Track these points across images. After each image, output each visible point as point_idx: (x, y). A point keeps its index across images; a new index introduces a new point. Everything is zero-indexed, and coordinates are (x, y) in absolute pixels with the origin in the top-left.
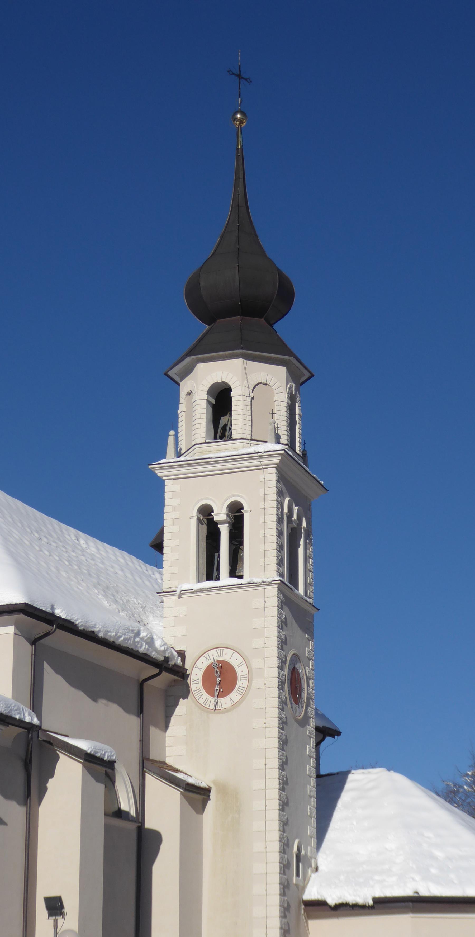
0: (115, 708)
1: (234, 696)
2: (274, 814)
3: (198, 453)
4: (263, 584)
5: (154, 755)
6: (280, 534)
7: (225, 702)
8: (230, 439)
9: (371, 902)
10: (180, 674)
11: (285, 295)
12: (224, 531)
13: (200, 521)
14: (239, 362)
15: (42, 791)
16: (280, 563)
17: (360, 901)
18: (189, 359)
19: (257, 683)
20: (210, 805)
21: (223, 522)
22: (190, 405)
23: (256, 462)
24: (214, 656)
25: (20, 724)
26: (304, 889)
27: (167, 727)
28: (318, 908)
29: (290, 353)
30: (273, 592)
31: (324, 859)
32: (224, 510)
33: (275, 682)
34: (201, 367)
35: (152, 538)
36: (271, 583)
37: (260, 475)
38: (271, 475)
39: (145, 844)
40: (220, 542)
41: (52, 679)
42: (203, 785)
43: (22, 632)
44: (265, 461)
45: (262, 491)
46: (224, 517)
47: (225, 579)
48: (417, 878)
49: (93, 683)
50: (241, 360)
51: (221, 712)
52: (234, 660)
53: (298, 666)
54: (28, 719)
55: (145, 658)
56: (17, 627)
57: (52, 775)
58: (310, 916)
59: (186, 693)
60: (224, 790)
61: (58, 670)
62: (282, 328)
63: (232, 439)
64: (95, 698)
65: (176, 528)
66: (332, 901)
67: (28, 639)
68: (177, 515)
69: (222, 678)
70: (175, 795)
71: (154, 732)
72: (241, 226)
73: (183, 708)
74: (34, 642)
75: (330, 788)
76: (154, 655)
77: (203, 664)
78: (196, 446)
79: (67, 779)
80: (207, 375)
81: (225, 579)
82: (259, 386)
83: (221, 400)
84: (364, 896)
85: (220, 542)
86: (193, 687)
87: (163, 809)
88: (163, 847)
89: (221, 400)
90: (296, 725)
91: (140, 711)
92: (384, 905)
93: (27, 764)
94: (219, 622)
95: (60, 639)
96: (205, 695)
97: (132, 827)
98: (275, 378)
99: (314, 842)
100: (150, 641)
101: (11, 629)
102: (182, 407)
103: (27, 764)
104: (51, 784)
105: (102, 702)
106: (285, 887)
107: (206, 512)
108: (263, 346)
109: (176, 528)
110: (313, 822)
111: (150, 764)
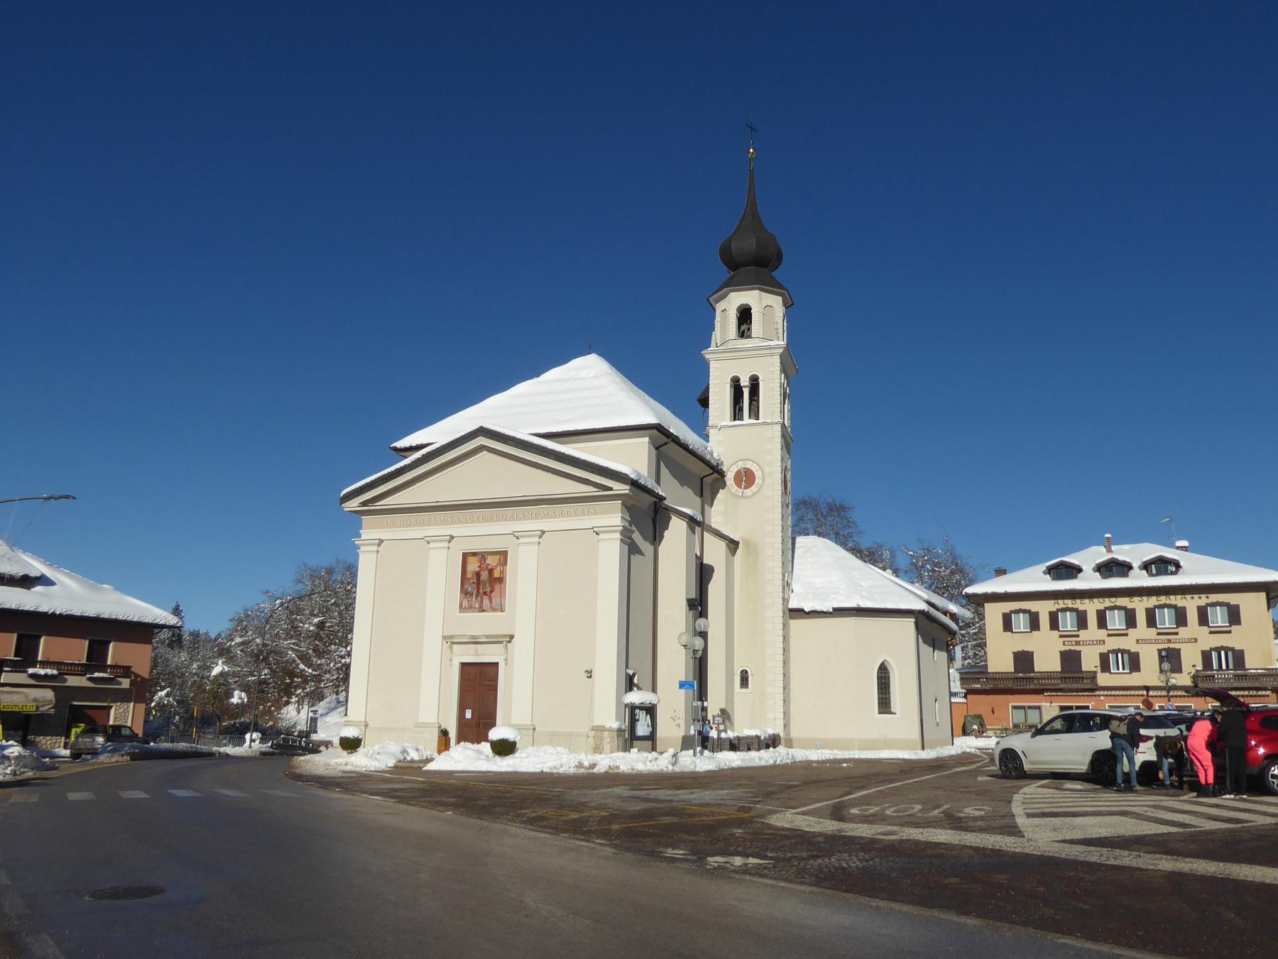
1: (754, 488)
3: (731, 345)
4: (772, 423)
7: (748, 492)
8: (750, 337)
10: (722, 474)
11: (779, 258)
14: (757, 292)
17: (825, 610)
19: (768, 481)
22: (725, 318)
24: (741, 465)
28: (797, 613)
29: (781, 287)
37: (770, 359)
38: (777, 360)
43: (652, 442)
47: (747, 420)
49: (682, 476)
52: (754, 468)
55: (707, 463)
59: (724, 485)
60: (747, 543)
63: (750, 340)
66: (807, 610)
69: (746, 478)
73: (721, 494)
74: (657, 448)
77: (734, 469)
78: (481, 441)
80: (736, 299)
81: (747, 420)
82: (767, 307)
83: (745, 315)
84: (827, 606)
85: (745, 397)
87: (715, 553)
89: (745, 315)
91: (701, 496)
92: (839, 612)
94: (748, 445)
95: (672, 448)
98: (776, 302)
100: (712, 454)
101: (647, 439)
102: (718, 319)
103: (654, 521)
104: (666, 533)
107: (736, 383)
108: (769, 284)
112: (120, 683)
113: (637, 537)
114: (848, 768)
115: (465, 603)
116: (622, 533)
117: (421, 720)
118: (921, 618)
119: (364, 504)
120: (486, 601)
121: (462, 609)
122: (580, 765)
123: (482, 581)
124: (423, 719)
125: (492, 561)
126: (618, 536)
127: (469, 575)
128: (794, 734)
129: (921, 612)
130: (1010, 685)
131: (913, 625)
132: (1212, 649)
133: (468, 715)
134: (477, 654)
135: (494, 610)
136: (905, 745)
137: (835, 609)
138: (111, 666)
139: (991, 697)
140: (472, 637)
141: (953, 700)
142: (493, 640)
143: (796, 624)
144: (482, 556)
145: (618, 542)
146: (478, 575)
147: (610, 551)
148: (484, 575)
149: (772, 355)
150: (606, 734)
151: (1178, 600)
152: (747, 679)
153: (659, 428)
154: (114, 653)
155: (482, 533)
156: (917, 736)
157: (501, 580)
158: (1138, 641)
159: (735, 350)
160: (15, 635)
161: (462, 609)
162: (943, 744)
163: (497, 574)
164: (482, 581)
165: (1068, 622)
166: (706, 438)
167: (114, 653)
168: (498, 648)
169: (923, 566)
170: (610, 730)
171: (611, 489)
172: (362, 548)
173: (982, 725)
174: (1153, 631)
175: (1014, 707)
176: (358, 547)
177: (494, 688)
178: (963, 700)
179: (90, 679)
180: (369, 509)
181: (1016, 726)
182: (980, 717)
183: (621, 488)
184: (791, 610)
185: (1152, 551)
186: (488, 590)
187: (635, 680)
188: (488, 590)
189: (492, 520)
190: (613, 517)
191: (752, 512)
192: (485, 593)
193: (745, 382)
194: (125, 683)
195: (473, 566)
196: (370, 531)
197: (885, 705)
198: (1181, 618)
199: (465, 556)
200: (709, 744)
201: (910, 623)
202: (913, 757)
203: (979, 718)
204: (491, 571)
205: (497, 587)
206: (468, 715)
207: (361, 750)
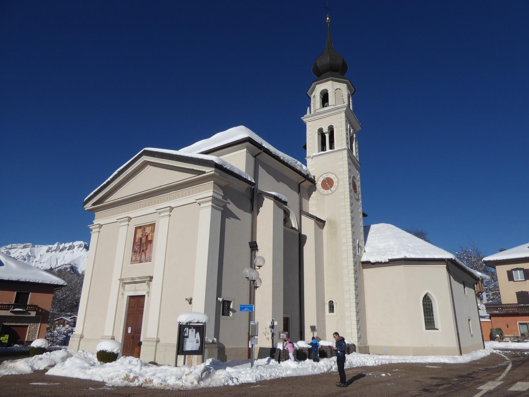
2: (349, 229)
5: (304, 209)
6: (347, 139)
9: (388, 261)
10: (313, 181)
12: (327, 136)
13: (319, 134)
15: (258, 212)
16: (347, 143)
19: (341, 183)
20: (325, 227)
21: (327, 133)
23: (338, 111)
24: (325, 176)
25: (246, 180)
26: (361, 258)
28: (367, 264)
30: (346, 152)
31: (367, 248)
33: (348, 182)
34: (317, 86)
36: (344, 149)
37: (339, 115)
38: (343, 115)
39: (302, 240)
40: (326, 140)
41: (262, 171)
43: (249, 151)
44: (341, 110)
45: (340, 120)
46: (327, 131)
48: (405, 252)
50: (331, 82)
52: (332, 177)
53: (355, 180)
54: (249, 179)
56: (247, 149)
57: (262, 206)
58: (364, 268)
61: (263, 167)
63: (330, 107)
64: (278, 181)
66: (372, 261)
67: (253, 156)
70: (312, 222)
71: (303, 199)
73: (314, 194)
74: (255, 157)
75: (366, 230)
76: (303, 172)
77: (321, 179)
79: (268, 205)
80: (320, 88)
81: (328, 150)
82: (338, 90)
85: (326, 140)
87: (308, 228)
88: (307, 241)
90: (355, 200)
91: (299, 192)
92: (393, 262)
93: (252, 201)
94: (330, 165)
97: (297, 233)
99: (363, 242)
102: (312, 102)
103: (252, 201)
104: (261, 209)
105: (281, 183)
106: (355, 255)
107: (321, 131)
110: (363, 235)
111: (302, 212)
112: (30, 314)
113: (232, 207)
114: (387, 380)
115: (133, 259)
116: (213, 202)
118: (449, 263)
119: (94, 204)
120: (143, 256)
121: (132, 262)
123: (142, 245)
124: (105, 334)
126: (210, 204)
127: (137, 241)
128: (371, 342)
129: (450, 260)
130: (516, 311)
131: (445, 269)
133: (129, 331)
134: (135, 290)
136: (447, 352)
138: (29, 305)
139: (506, 318)
140: (133, 279)
141: (482, 320)
143: (367, 272)
145: (210, 209)
146: (141, 239)
147: (205, 217)
148: (144, 239)
149: (340, 113)
152: (333, 307)
153: (249, 140)
154: (32, 298)
155: (141, 213)
156: (455, 345)
157: (151, 242)
159: (319, 114)
160: (16, 292)
162: (476, 348)
163: (149, 238)
164: (142, 245)
166: (305, 163)
167: (32, 298)
168: (144, 285)
169: (463, 258)
171: (204, 172)
172: (93, 231)
173: (501, 335)
175: (520, 324)
176: (91, 230)
177: (273, 315)
178: (489, 320)
179: (11, 312)
181: (523, 335)
182: (500, 330)
183: (209, 171)
184: (364, 263)
187: (231, 307)
188: (145, 248)
189: (149, 205)
190: (207, 191)
191: (334, 204)
192: (143, 251)
193: (326, 130)
194: (33, 314)
196: (100, 219)
197: (430, 323)
200: (276, 354)
201: (442, 269)
202: (452, 362)
203: (499, 331)
204: (147, 237)
205: (149, 246)
206: (129, 331)
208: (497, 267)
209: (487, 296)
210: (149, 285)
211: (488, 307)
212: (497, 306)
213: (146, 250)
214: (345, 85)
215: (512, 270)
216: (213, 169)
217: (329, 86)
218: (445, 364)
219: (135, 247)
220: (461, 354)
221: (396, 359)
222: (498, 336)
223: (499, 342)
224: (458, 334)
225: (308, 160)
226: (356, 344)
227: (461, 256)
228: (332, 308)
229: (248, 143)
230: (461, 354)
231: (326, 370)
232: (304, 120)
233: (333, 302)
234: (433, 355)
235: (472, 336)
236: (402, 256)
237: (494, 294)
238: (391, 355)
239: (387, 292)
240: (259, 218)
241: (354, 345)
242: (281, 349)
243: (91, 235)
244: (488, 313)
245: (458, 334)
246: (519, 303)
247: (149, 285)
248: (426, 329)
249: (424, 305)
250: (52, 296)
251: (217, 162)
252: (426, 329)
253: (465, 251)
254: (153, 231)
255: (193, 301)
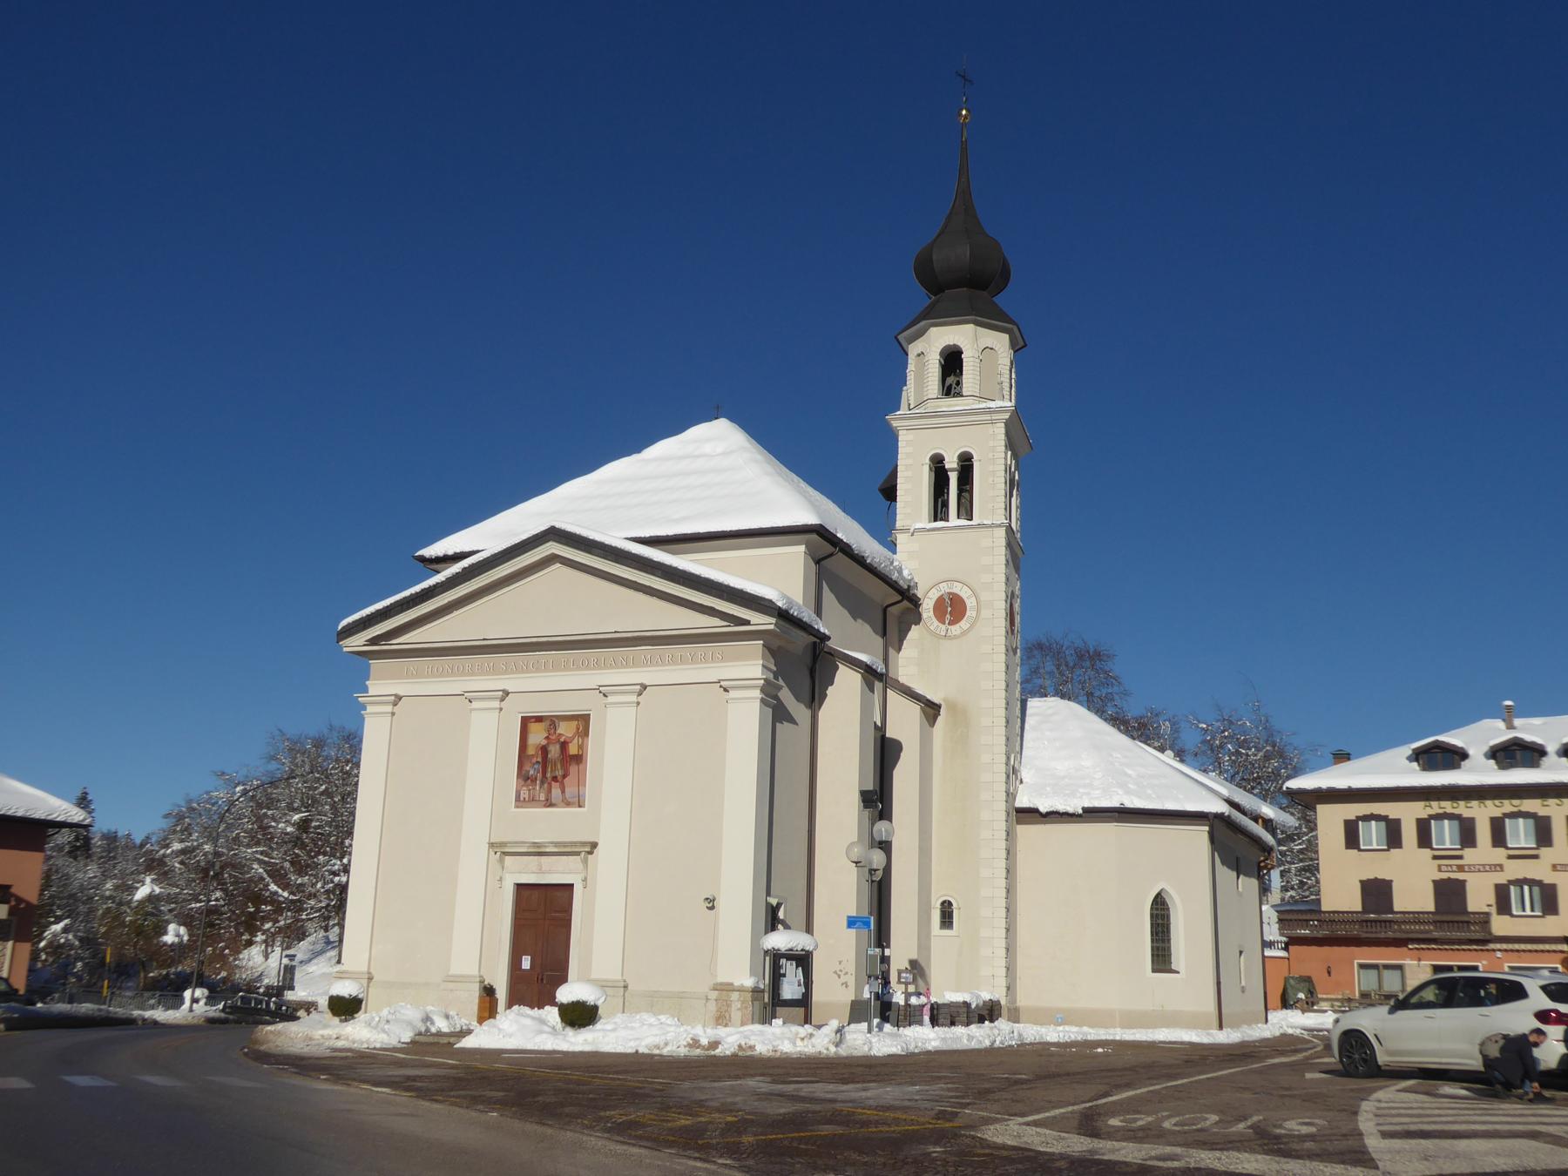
0: (867, 628)
1: (964, 624)
3: (931, 407)
4: (992, 526)
8: (959, 395)
10: (915, 602)
11: (1005, 275)
12: (953, 478)
14: (969, 328)
17: (1071, 810)
18: (923, 323)
19: (985, 613)
22: (922, 367)
23: (987, 417)
24: (944, 588)
27: (900, 649)
28: (1029, 815)
29: (1010, 321)
32: (955, 459)
34: (933, 330)
35: (880, 480)
38: (1000, 430)
42: (936, 701)
43: (811, 552)
44: (995, 416)
46: (955, 465)
47: (954, 521)
49: (856, 606)
51: (951, 638)
52: (964, 593)
55: (893, 585)
59: (918, 619)
60: (953, 707)
62: (999, 300)
63: (959, 400)
65: (909, 474)
66: (1043, 810)
68: (910, 461)
69: (952, 608)
70: (915, 709)
71: (891, 651)
72: (964, 211)
73: (914, 633)
74: (818, 562)
77: (934, 595)
80: (939, 338)
81: (954, 521)
82: (985, 348)
83: (952, 362)
84: (1075, 806)
86: (925, 615)
87: (903, 721)
89: (952, 362)
91: (884, 634)
92: (1093, 814)
94: (957, 558)
95: (839, 562)
96: (936, 623)
98: (1000, 342)
100: (900, 571)
102: (911, 367)
104: (830, 690)
107: (938, 464)
108: (991, 316)
109: (909, 474)
114: (1105, 1055)
115: (525, 794)
116: (763, 690)
117: (453, 971)
120: (556, 791)
122: (695, 1043)
123: (550, 760)
124: (456, 969)
125: (566, 730)
126: (757, 694)
127: (531, 751)
128: (1022, 1001)
130: (1355, 931)
131: (1206, 835)
132: (1511, 882)
133: (526, 963)
134: (541, 872)
135: (568, 804)
136: (1193, 1022)
137: (1087, 811)
139: (1326, 949)
141: (1268, 953)
142: (566, 850)
144: (551, 722)
145: (757, 704)
146: (544, 750)
148: (554, 751)
150: (735, 996)
151: (1463, 809)
153: (820, 531)
155: (551, 687)
156: (1211, 1007)
157: (579, 759)
158: (1554, 867)
159: (936, 414)
161: (520, 802)
162: (1250, 1020)
163: (573, 749)
164: (550, 760)
165: (1445, 835)
166: (892, 546)
169: (1222, 746)
170: (741, 990)
171: (747, 623)
172: (370, 709)
173: (1311, 992)
174: (1501, 852)
175: (1362, 966)
178: (1283, 954)
180: (381, 649)
184: (1020, 811)
185: (1495, 731)
186: (559, 773)
187: (781, 915)
188: (559, 773)
191: (961, 662)
192: (555, 779)
193: (951, 463)
195: (537, 736)
196: (382, 683)
197: (1162, 958)
198: (1467, 835)
199: (525, 721)
200: (892, 1014)
202: (1205, 1040)
203: (1308, 983)
204: (564, 746)
205: (573, 769)
206: (526, 963)
207: (361, 1016)
208: (1319, 807)
209: (1283, 874)
210: (585, 862)
211: (1286, 918)
212: (1308, 917)
213: (564, 776)
214: (1006, 337)
215: (1359, 818)
216: (773, 620)
217: (963, 335)
218: (1193, 1046)
219: (527, 767)
220: (1221, 1027)
221: (1093, 1034)
222: (1301, 996)
223: (1304, 1011)
224: (1219, 983)
225: (901, 539)
226: (1003, 1002)
227: (1213, 738)
228: (947, 918)
229: (815, 536)
230: (1221, 1027)
231: (987, 1043)
232: (894, 424)
233: (950, 904)
234: (1168, 1026)
235: (1243, 990)
236: (1114, 803)
237: (1304, 869)
238: (1080, 1026)
239: (1064, 883)
240: (825, 713)
241: (998, 1003)
242: (902, 1003)
243: (363, 719)
244: (1282, 935)
245: (1219, 983)
246: (1365, 910)
247: (585, 862)
248: (1154, 971)
249: (1152, 916)
250: (39, 856)
251: (780, 604)
252: (1154, 971)
253: (1231, 723)
254: (584, 732)
255: (719, 904)
